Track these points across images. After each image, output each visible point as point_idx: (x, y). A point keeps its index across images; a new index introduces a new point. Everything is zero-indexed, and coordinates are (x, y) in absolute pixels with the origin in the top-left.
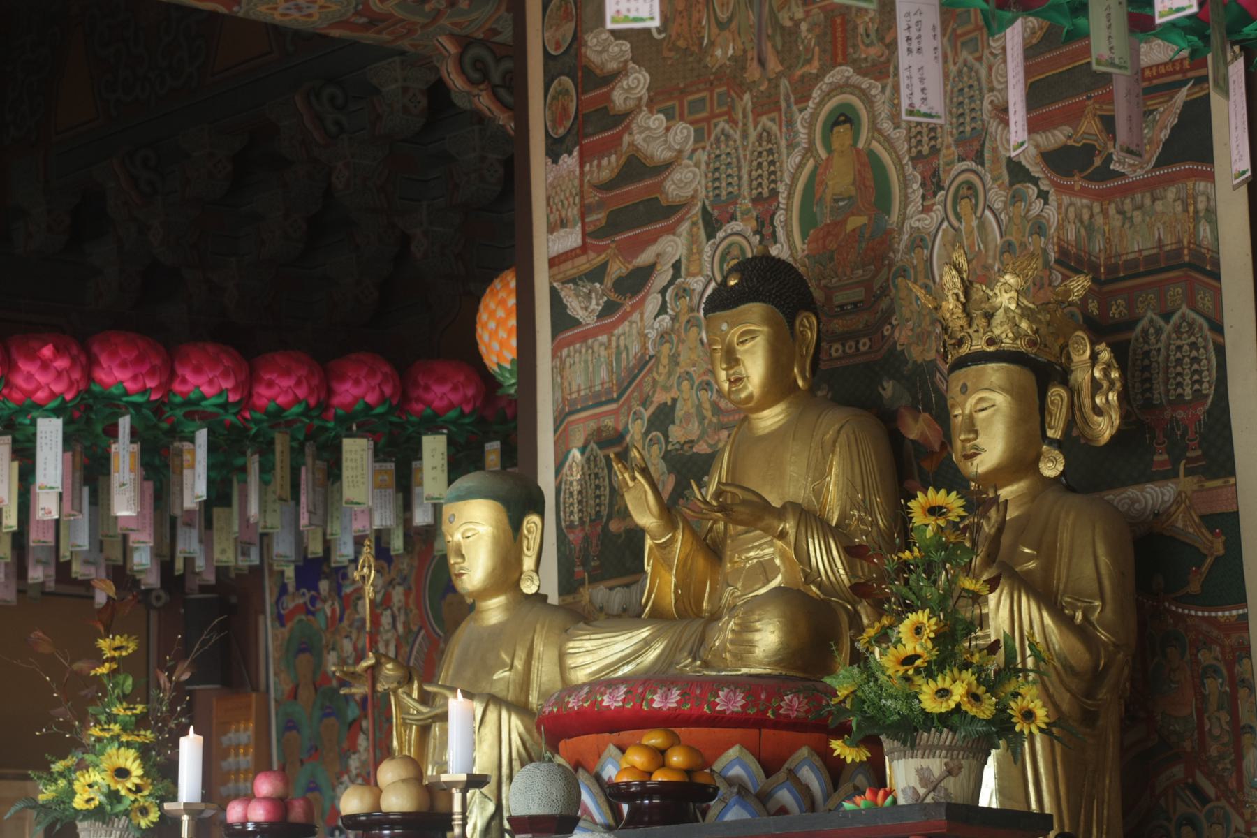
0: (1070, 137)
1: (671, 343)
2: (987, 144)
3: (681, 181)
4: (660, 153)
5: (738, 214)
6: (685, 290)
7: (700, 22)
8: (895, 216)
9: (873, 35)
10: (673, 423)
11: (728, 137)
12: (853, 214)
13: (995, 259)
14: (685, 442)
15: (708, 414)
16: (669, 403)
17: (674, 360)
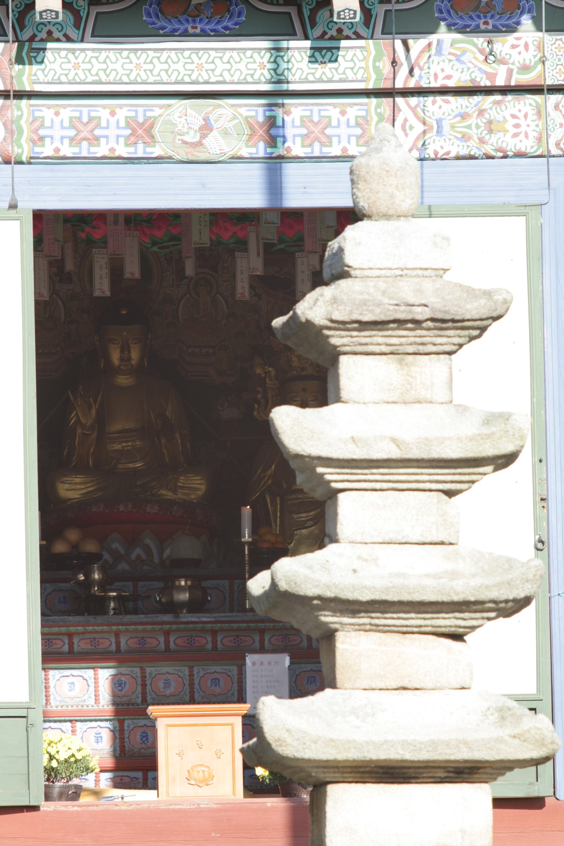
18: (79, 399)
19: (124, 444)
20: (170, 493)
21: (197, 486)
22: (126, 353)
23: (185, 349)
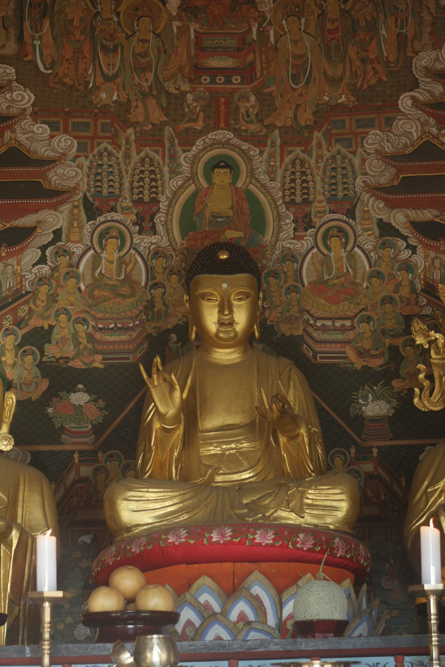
0: (437, 217)
1: (50, 285)
2: (359, 206)
3: (64, 174)
4: (43, 151)
5: (118, 208)
6: (65, 251)
7: (86, 70)
8: (268, 237)
9: (253, 117)
10: (50, 342)
11: (110, 154)
12: (230, 229)
13: (363, 279)
14: (61, 358)
15: (84, 341)
16: (46, 327)
17: (53, 298)
18: (155, 376)
19: (224, 447)
20: (293, 516)
21: (335, 504)
22: (226, 312)
23: (312, 322)
